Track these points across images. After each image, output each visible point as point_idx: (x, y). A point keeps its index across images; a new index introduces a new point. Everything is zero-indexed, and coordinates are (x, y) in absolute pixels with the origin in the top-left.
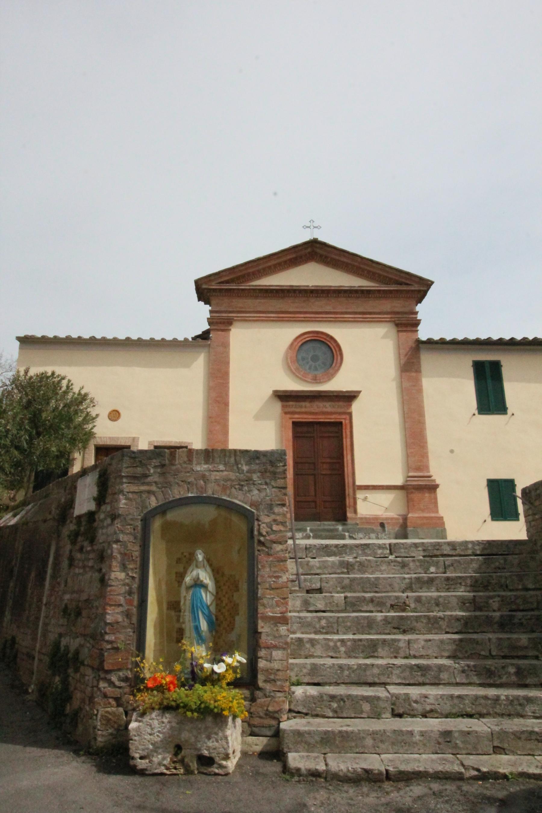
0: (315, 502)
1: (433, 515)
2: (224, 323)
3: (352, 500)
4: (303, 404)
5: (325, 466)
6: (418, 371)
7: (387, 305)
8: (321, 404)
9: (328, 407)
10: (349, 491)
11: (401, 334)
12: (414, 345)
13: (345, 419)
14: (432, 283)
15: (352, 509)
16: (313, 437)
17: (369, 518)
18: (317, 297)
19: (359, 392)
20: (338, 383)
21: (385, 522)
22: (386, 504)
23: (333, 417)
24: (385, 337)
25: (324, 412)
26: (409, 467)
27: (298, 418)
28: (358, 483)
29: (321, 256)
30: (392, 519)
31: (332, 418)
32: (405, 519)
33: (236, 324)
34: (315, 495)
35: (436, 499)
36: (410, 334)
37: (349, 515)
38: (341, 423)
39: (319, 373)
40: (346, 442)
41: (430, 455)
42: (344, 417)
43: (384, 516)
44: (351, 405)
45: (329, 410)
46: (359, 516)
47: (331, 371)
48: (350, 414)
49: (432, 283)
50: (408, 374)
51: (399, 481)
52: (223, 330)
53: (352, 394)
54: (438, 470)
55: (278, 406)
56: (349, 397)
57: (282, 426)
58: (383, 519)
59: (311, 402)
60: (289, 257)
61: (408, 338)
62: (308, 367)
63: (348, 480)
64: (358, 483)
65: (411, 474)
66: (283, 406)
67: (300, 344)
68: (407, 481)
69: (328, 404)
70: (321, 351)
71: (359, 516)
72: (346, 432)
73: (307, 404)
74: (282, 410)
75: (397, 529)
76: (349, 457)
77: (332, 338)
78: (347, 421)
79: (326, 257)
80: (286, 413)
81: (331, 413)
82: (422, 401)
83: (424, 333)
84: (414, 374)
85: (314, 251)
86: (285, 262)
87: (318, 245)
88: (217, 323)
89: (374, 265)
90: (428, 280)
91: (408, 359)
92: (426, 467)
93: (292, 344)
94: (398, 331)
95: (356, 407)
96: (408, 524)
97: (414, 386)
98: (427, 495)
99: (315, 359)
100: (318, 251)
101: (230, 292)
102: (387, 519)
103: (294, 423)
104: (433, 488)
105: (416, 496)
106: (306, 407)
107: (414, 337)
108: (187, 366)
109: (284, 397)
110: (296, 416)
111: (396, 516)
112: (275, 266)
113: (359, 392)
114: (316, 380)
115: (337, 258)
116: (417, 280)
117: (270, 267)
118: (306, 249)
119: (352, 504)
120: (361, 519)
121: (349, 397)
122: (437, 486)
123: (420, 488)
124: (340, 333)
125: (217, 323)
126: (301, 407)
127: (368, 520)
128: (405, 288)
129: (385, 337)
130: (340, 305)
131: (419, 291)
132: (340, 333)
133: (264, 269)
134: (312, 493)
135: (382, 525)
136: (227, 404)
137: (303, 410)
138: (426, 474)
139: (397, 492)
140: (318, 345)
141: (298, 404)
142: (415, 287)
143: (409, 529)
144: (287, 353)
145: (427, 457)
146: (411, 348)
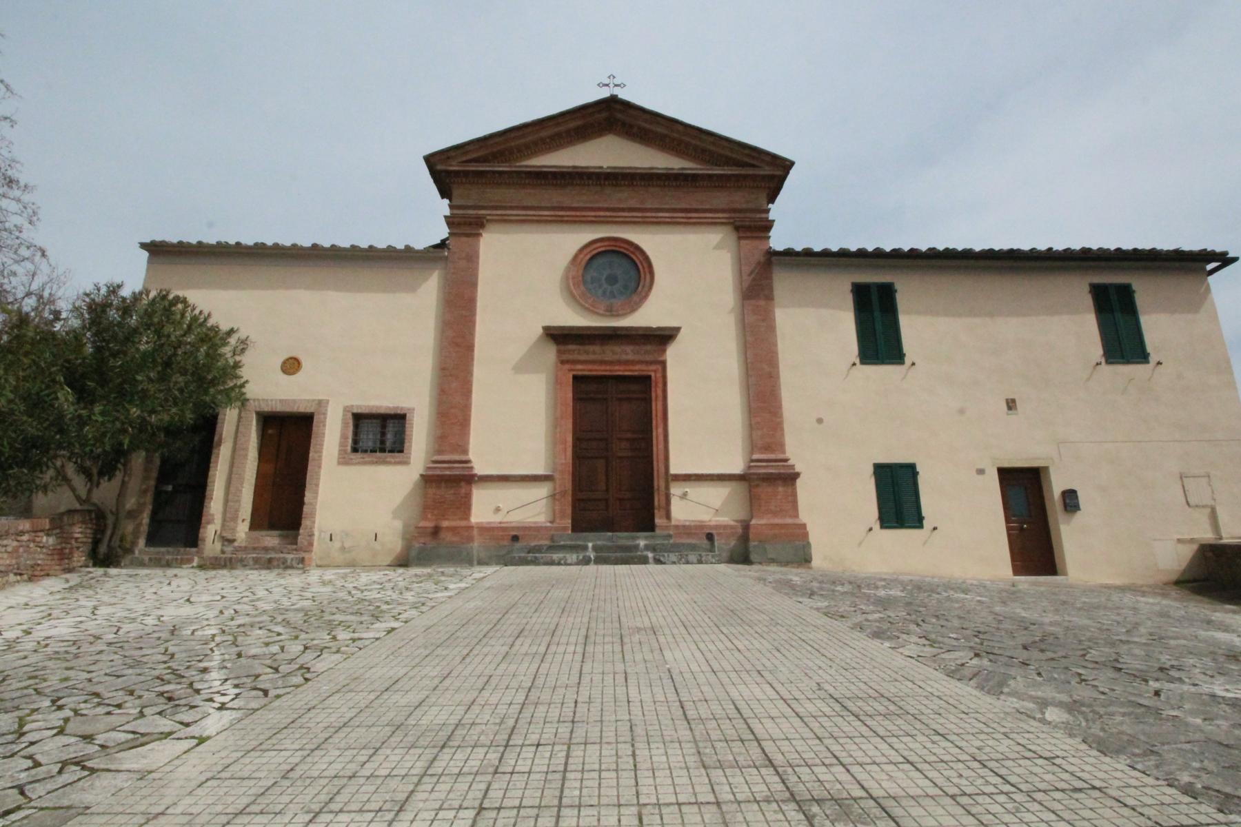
0: (607, 500)
1: (789, 521)
2: (470, 224)
3: (663, 498)
4: (591, 348)
5: (624, 444)
6: (770, 298)
7: (721, 199)
8: (617, 349)
9: (628, 352)
10: (659, 482)
11: (743, 242)
12: (762, 259)
13: (655, 371)
14: (792, 163)
15: (663, 512)
16: (605, 399)
17: (689, 527)
18: (616, 185)
19: (678, 329)
20: (647, 316)
21: (714, 532)
22: (717, 503)
23: (637, 367)
24: (717, 247)
25: (621, 361)
26: (752, 446)
27: (582, 369)
28: (673, 471)
29: (624, 124)
30: (725, 527)
31: (636, 370)
32: (746, 526)
33: (490, 227)
34: (607, 490)
35: (794, 495)
36: (756, 243)
37: (658, 521)
38: (649, 377)
39: (617, 303)
40: (656, 406)
41: (786, 426)
42: (653, 367)
43: (713, 523)
44: (664, 351)
45: (630, 357)
46: (673, 523)
47: (635, 298)
48: (663, 364)
49: (792, 163)
50: (753, 302)
51: (737, 467)
52: (468, 235)
53: (667, 333)
54: (799, 450)
55: (550, 353)
56: (663, 337)
57: (557, 382)
58: (711, 527)
59: (602, 344)
60: (572, 125)
61: (754, 249)
62: (600, 292)
63: (658, 466)
64: (673, 471)
65: (755, 457)
66: (559, 352)
67: (588, 257)
68: (750, 467)
69: (629, 349)
70: (620, 268)
71: (673, 523)
72: (656, 392)
73: (597, 348)
74: (558, 357)
75: (733, 543)
76: (660, 430)
77: (638, 248)
78: (659, 375)
79: (631, 126)
80: (563, 362)
81: (633, 363)
82: (776, 345)
83: (778, 240)
84: (762, 303)
85: (611, 116)
86: (568, 132)
87: (618, 107)
88: (459, 224)
89: (704, 137)
90: (786, 160)
91: (754, 280)
92: (781, 446)
93: (576, 256)
94: (740, 238)
95: (672, 354)
96: (751, 536)
97: (763, 320)
98: (780, 489)
99: (612, 280)
100: (619, 116)
101: (485, 176)
102: (717, 527)
103: (575, 377)
104: (791, 478)
105: (764, 490)
106: (594, 353)
107: (763, 247)
108: (412, 288)
109: (559, 337)
110: (580, 367)
111: (733, 523)
112: (552, 138)
113: (678, 329)
114: (611, 312)
115: (647, 126)
116: (768, 159)
117: (543, 140)
118: (599, 112)
119: (663, 502)
120: (677, 527)
121: (663, 337)
122: (797, 475)
123: (770, 479)
124: (650, 241)
125: (459, 224)
126: (587, 353)
127: (687, 530)
128: (750, 171)
129: (717, 247)
130: (651, 198)
131: (772, 177)
132: (650, 241)
133: (535, 143)
134: (602, 486)
135: (710, 537)
136: (470, 348)
137: (591, 357)
138: (781, 456)
139: (734, 484)
140: (616, 260)
141: (581, 348)
142: (767, 171)
143: (752, 544)
144: (568, 270)
145: (782, 429)
146: (759, 263)
